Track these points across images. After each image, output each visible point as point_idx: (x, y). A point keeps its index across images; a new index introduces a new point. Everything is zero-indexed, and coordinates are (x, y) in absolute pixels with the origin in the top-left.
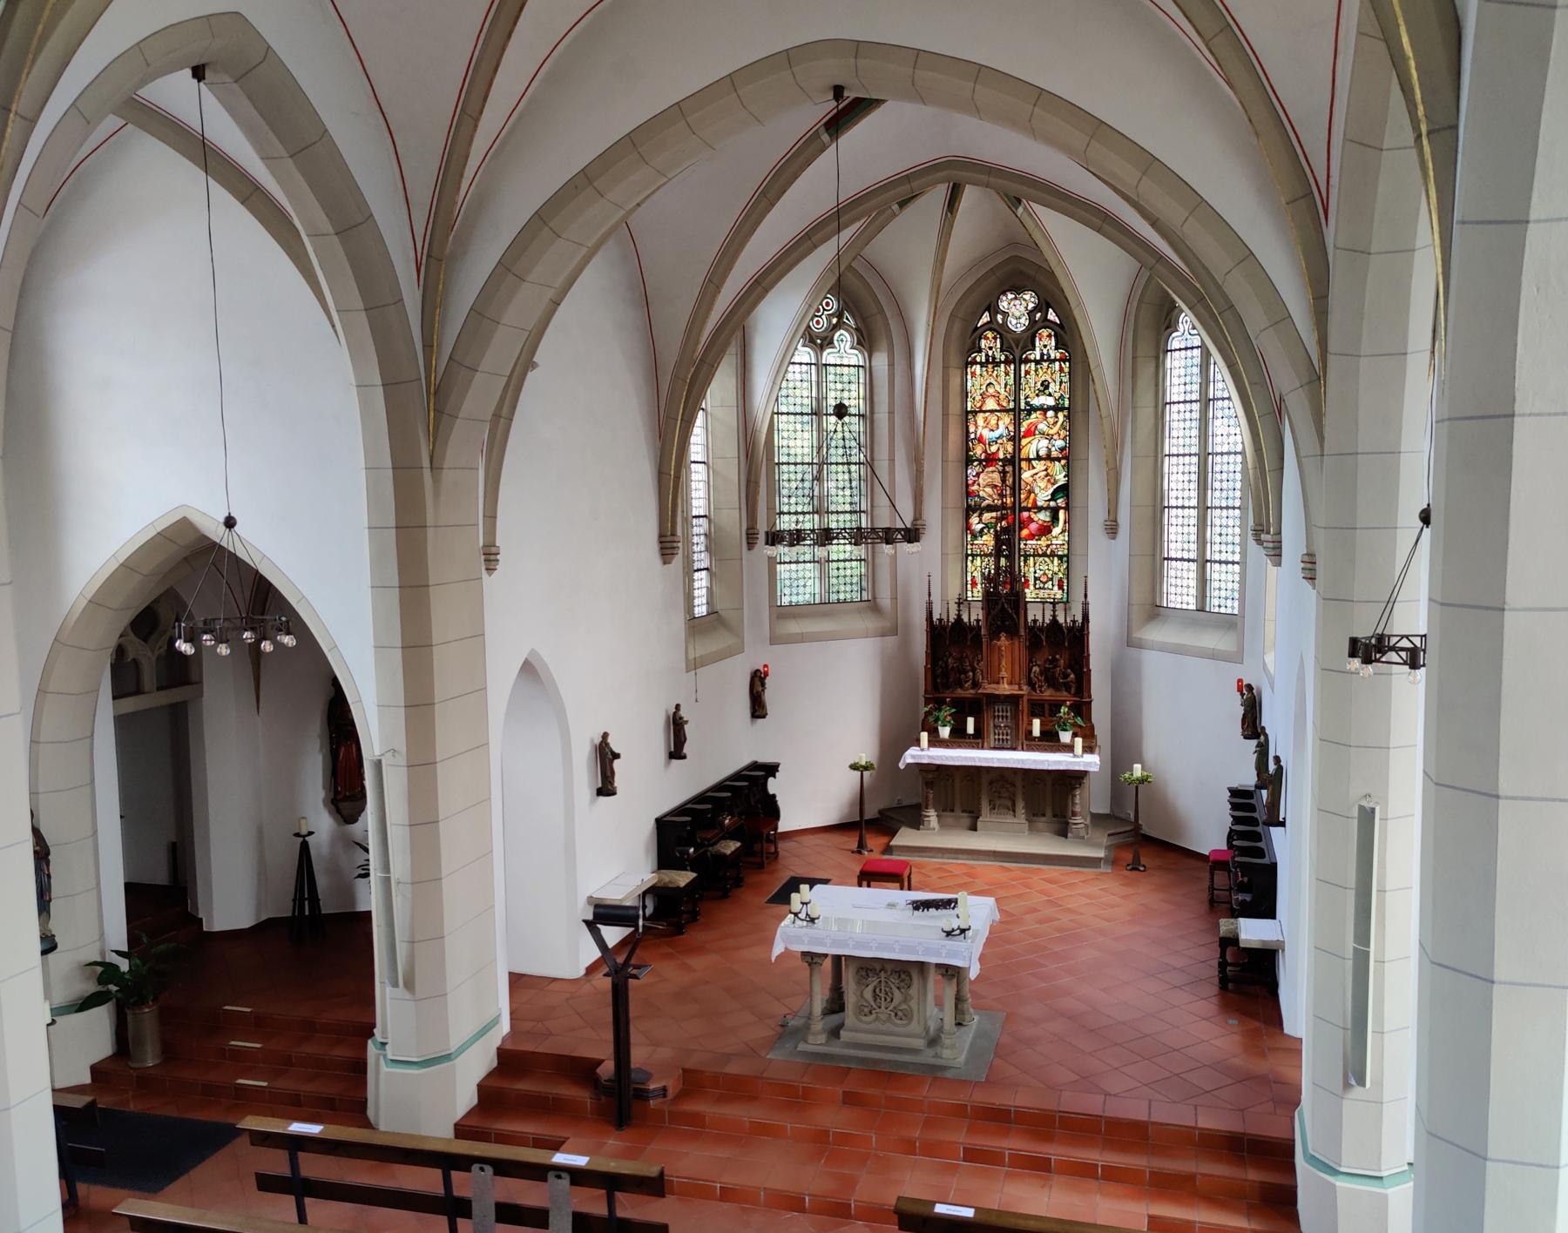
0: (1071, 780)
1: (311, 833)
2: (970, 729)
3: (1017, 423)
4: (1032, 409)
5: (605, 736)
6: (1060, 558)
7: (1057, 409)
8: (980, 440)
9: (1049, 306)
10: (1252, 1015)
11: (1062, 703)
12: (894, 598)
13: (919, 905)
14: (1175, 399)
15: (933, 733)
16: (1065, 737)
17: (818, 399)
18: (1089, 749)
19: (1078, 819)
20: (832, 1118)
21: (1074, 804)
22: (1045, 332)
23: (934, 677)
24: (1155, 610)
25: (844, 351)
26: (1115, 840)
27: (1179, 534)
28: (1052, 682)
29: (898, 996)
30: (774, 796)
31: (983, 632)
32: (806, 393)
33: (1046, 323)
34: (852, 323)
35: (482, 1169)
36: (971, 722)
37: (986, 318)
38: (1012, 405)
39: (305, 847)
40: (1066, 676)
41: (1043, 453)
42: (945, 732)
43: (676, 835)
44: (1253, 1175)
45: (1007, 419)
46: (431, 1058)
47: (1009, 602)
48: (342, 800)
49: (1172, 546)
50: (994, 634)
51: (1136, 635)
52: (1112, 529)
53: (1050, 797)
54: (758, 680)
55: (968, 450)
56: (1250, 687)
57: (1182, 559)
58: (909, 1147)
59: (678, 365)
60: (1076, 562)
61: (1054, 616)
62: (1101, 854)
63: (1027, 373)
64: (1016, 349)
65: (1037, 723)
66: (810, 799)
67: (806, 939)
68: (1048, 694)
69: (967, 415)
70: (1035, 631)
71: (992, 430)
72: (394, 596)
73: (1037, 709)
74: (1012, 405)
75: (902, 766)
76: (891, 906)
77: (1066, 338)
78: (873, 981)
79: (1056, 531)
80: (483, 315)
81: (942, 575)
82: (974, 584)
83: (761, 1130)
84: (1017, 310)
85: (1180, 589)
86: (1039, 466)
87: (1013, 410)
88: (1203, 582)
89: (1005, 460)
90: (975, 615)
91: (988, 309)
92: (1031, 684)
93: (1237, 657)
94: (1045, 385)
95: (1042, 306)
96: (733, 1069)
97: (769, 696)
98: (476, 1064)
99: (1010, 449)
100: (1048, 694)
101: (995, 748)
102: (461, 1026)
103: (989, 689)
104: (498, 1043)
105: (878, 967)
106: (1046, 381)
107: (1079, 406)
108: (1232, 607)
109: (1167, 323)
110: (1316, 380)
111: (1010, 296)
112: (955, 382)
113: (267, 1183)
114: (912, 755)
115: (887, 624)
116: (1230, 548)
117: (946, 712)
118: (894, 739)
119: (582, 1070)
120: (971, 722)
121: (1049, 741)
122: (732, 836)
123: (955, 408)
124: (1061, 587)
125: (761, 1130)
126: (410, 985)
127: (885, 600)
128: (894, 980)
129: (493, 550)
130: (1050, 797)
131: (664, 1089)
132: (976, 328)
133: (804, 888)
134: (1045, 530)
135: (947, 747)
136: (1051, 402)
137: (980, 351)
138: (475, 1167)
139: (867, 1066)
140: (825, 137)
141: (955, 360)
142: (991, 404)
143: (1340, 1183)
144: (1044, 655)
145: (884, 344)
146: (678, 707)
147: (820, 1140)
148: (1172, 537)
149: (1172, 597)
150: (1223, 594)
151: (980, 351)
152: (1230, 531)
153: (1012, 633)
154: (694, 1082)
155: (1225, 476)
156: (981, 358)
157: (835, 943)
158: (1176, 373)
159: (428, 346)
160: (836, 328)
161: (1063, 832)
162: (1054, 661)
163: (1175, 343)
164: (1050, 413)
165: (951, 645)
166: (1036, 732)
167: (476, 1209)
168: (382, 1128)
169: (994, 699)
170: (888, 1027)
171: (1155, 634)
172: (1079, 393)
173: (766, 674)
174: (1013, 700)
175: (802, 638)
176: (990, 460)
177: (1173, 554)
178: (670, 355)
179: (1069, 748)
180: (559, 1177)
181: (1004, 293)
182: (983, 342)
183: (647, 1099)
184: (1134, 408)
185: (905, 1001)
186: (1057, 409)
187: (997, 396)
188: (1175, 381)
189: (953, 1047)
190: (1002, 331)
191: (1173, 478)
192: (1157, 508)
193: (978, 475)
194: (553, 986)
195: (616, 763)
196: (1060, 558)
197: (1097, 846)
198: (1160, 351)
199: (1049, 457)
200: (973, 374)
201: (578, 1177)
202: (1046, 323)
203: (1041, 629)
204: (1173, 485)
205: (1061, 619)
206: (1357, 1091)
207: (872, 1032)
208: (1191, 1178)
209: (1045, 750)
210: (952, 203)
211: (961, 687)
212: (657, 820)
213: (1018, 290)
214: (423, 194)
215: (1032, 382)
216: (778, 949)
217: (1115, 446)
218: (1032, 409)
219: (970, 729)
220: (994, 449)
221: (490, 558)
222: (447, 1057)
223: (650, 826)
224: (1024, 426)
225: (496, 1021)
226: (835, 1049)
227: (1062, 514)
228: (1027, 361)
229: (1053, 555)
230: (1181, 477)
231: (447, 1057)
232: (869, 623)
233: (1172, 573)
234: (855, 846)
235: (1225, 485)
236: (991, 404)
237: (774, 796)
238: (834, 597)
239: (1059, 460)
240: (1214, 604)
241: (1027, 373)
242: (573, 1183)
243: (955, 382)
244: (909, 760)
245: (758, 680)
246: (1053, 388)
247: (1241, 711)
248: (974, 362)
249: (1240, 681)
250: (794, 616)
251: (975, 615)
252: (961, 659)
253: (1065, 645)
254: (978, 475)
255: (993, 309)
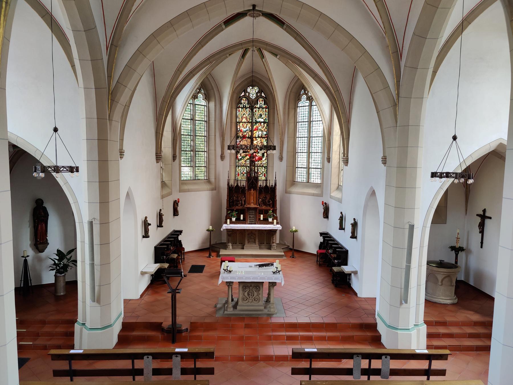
0: (273, 232)
1: (28, 256)
2: (242, 218)
3: (252, 126)
4: (256, 122)
5: (146, 218)
6: (265, 167)
7: (264, 122)
8: (241, 131)
9: (262, 91)
10: (348, 293)
11: (270, 210)
12: (215, 179)
13: (260, 266)
14: (300, 121)
15: (231, 219)
16: (270, 220)
17: (193, 115)
18: (277, 223)
19: (275, 244)
20: (243, 332)
21: (273, 240)
22: (261, 99)
23: (230, 202)
24: (293, 182)
25: (201, 100)
26: (285, 250)
27: (301, 160)
28: (265, 204)
29: (256, 294)
30: (181, 241)
31: (246, 188)
32: (189, 113)
33: (261, 97)
34: (203, 92)
35: (148, 358)
36: (242, 216)
37: (243, 94)
38: (251, 121)
39: (26, 261)
40: (269, 202)
41: (260, 135)
42: (234, 219)
43: (160, 253)
44: (369, 334)
45: (249, 125)
46: (97, 327)
47: (254, 179)
48: (39, 244)
49: (299, 164)
50: (249, 189)
51: (288, 190)
52: (281, 159)
53: (266, 238)
54: (176, 204)
55: (237, 134)
56: (326, 203)
57: (302, 168)
58: (270, 338)
59: (164, 97)
60: (270, 168)
61: (266, 184)
62: (283, 254)
63: (256, 111)
64: (252, 105)
65: (262, 216)
66: (190, 242)
67: (229, 278)
68: (264, 207)
69: (237, 123)
70: (261, 188)
71: (245, 128)
72: (96, 164)
73: (261, 212)
74: (251, 121)
75: (222, 230)
76: (251, 267)
77: (267, 101)
78: (248, 290)
79: (264, 159)
80: (130, 67)
81: (230, 171)
82: (238, 175)
83: (220, 338)
84: (253, 92)
85: (301, 176)
86: (259, 139)
87: (251, 122)
88: (308, 174)
89: (248, 138)
90: (244, 183)
91: (244, 91)
92: (259, 205)
93: (321, 195)
94: (261, 115)
95: (260, 91)
96: (207, 320)
97: (179, 209)
98: (117, 328)
99: (250, 134)
100: (264, 207)
101: (249, 224)
102: (114, 315)
103: (248, 206)
104: (122, 321)
105: (249, 285)
106: (261, 114)
107: (271, 122)
108: (319, 181)
109: (299, 99)
110: (395, 105)
111: (251, 88)
112: (234, 113)
113: (57, 373)
114: (225, 227)
115: (213, 187)
116: (317, 164)
117: (234, 213)
118: (216, 222)
119: (157, 326)
120: (242, 216)
121: (265, 221)
122: (174, 252)
123: (234, 121)
124: (265, 176)
125: (220, 338)
126: (98, 301)
127: (212, 179)
128: (254, 290)
129: (123, 151)
130: (266, 238)
131: (187, 329)
132: (240, 97)
133: (227, 262)
134: (260, 159)
135: (235, 224)
136: (262, 120)
137: (241, 104)
138: (145, 357)
139: (248, 317)
140: (224, 26)
141: (234, 106)
142: (244, 120)
143: (399, 332)
144: (263, 195)
145: (213, 99)
146: (160, 210)
147: (241, 339)
148: (299, 161)
149: (299, 179)
150: (315, 177)
151: (241, 104)
152: (317, 159)
153: (255, 188)
154: (194, 326)
155: (316, 143)
156: (241, 106)
157: (239, 278)
158: (300, 113)
159: (110, 77)
160: (198, 93)
161: (270, 248)
162: (266, 197)
163: (300, 104)
164: (262, 124)
165: (235, 192)
166: (262, 219)
167: (145, 372)
168: (359, 295)
169: (249, 209)
170: (252, 304)
171: (294, 189)
172: (271, 119)
173: (179, 202)
174: (255, 209)
175: (189, 191)
176: (244, 137)
177: (299, 166)
178: (162, 93)
179: (272, 223)
180: (177, 356)
181: (249, 86)
182: (242, 101)
183: (182, 332)
184: (288, 123)
185: (258, 295)
186: (264, 122)
187: (246, 118)
188: (300, 116)
189: (274, 308)
190: (248, 98)
191: (299, 144)
192: (294, 153)
193: (240, 142)
194: (130, 302)
195: (149, 227)
196: (265, 167)
197: (281, 252)
198: (296, 107)
199: (262, 137)
200: (239, 111)
201: (183, 355)
202: (261, 97)
203: (262, 188)
204: (299, 146)
205: (268, 185)
206: (404, 305)
207: (247, 306)
208: (353, 336)
209: (264, 224)
210: (244, 55)
211: (238, 205)
212: (155, 247)
213: (253, 86)
214: (111, 22)
215: (257, 112)
216: (220, 281)
217: (282, 134)
218: (256, 122)
219: (242, 218)
220: (245, 134)
221: (122, 153)
222: (110, 326)
223: (153, 249)
224: (255, 127)
225: (121, 314)
226: (236, 312)
227: (265, 154)
228: (256, 108)
229: (262, 166)
230: (302, 144)
231: (110, 326)
232: (207, 186)
233: (299, 172)
234: (208, 255)
235: (316, 146)
236: (244, 120)
237: (181, 241)
238: (197, 178)
239: (265, 138)
240: (312, 180)
241: (256, 111)
242: (182, 358)
243: (234, 113)
244: (224, 228)
245: (176, 204)
246: (263, 116)
247: (323, 211)
248: (239, 107)
249: (323, 202)
250: (185, 184)
251: (244, 183)
252: (238, 197)
253: (269, 192)
254: (240, 142)
255: (245, 91)
